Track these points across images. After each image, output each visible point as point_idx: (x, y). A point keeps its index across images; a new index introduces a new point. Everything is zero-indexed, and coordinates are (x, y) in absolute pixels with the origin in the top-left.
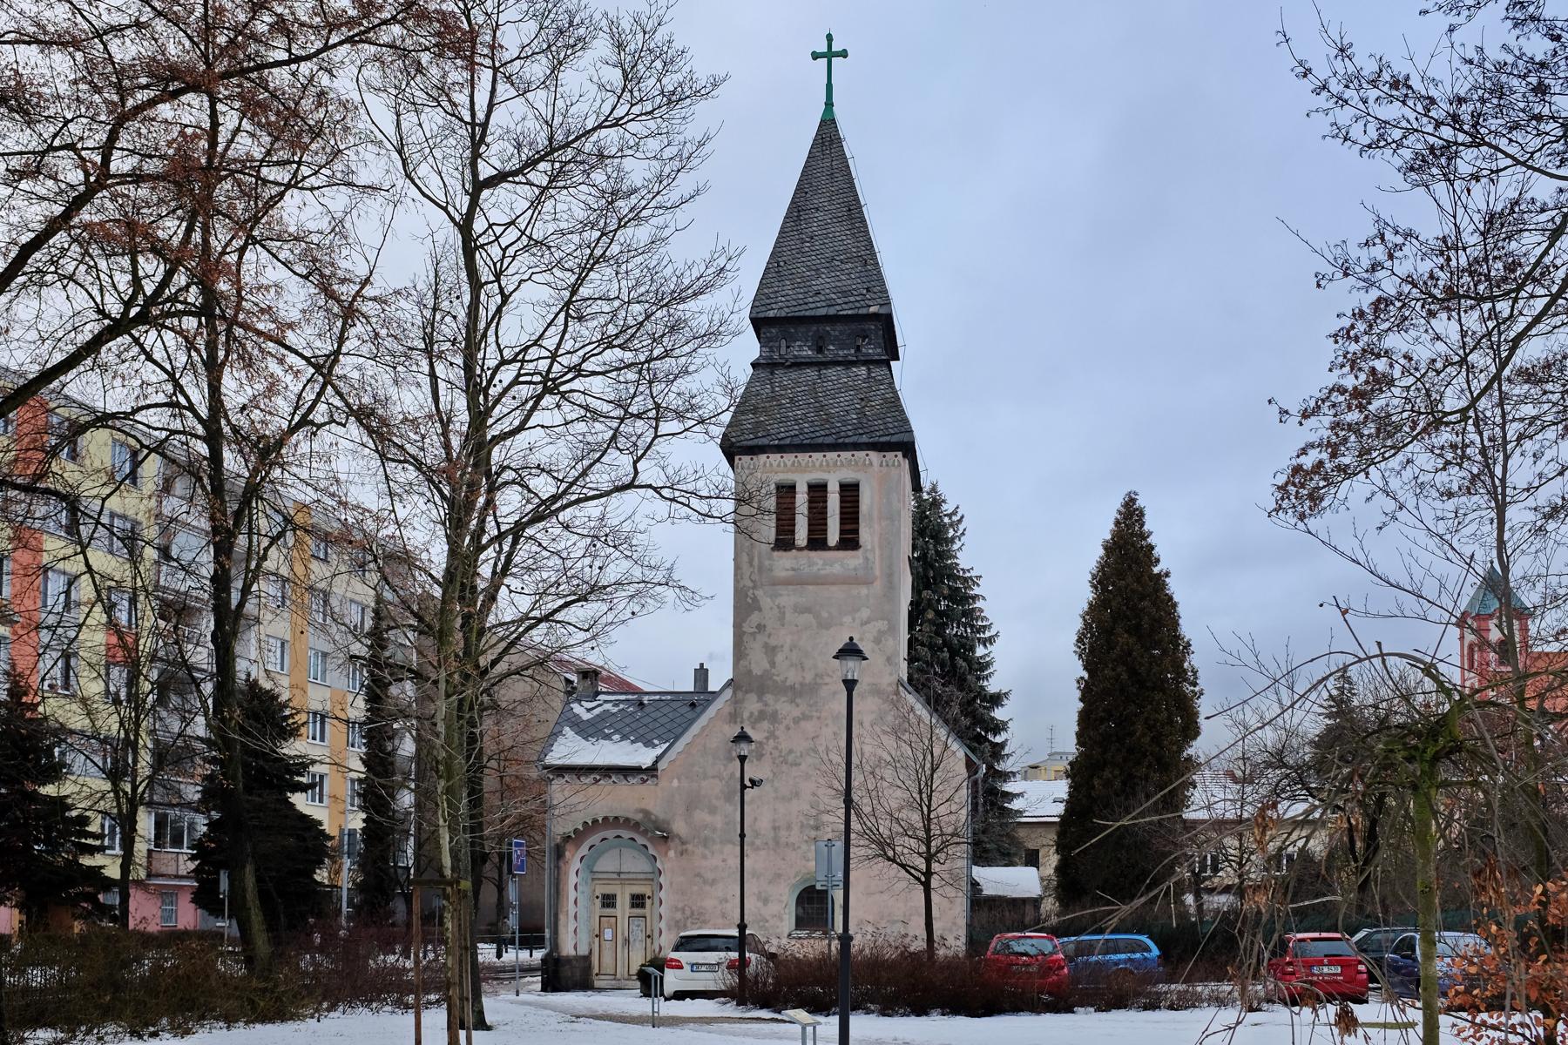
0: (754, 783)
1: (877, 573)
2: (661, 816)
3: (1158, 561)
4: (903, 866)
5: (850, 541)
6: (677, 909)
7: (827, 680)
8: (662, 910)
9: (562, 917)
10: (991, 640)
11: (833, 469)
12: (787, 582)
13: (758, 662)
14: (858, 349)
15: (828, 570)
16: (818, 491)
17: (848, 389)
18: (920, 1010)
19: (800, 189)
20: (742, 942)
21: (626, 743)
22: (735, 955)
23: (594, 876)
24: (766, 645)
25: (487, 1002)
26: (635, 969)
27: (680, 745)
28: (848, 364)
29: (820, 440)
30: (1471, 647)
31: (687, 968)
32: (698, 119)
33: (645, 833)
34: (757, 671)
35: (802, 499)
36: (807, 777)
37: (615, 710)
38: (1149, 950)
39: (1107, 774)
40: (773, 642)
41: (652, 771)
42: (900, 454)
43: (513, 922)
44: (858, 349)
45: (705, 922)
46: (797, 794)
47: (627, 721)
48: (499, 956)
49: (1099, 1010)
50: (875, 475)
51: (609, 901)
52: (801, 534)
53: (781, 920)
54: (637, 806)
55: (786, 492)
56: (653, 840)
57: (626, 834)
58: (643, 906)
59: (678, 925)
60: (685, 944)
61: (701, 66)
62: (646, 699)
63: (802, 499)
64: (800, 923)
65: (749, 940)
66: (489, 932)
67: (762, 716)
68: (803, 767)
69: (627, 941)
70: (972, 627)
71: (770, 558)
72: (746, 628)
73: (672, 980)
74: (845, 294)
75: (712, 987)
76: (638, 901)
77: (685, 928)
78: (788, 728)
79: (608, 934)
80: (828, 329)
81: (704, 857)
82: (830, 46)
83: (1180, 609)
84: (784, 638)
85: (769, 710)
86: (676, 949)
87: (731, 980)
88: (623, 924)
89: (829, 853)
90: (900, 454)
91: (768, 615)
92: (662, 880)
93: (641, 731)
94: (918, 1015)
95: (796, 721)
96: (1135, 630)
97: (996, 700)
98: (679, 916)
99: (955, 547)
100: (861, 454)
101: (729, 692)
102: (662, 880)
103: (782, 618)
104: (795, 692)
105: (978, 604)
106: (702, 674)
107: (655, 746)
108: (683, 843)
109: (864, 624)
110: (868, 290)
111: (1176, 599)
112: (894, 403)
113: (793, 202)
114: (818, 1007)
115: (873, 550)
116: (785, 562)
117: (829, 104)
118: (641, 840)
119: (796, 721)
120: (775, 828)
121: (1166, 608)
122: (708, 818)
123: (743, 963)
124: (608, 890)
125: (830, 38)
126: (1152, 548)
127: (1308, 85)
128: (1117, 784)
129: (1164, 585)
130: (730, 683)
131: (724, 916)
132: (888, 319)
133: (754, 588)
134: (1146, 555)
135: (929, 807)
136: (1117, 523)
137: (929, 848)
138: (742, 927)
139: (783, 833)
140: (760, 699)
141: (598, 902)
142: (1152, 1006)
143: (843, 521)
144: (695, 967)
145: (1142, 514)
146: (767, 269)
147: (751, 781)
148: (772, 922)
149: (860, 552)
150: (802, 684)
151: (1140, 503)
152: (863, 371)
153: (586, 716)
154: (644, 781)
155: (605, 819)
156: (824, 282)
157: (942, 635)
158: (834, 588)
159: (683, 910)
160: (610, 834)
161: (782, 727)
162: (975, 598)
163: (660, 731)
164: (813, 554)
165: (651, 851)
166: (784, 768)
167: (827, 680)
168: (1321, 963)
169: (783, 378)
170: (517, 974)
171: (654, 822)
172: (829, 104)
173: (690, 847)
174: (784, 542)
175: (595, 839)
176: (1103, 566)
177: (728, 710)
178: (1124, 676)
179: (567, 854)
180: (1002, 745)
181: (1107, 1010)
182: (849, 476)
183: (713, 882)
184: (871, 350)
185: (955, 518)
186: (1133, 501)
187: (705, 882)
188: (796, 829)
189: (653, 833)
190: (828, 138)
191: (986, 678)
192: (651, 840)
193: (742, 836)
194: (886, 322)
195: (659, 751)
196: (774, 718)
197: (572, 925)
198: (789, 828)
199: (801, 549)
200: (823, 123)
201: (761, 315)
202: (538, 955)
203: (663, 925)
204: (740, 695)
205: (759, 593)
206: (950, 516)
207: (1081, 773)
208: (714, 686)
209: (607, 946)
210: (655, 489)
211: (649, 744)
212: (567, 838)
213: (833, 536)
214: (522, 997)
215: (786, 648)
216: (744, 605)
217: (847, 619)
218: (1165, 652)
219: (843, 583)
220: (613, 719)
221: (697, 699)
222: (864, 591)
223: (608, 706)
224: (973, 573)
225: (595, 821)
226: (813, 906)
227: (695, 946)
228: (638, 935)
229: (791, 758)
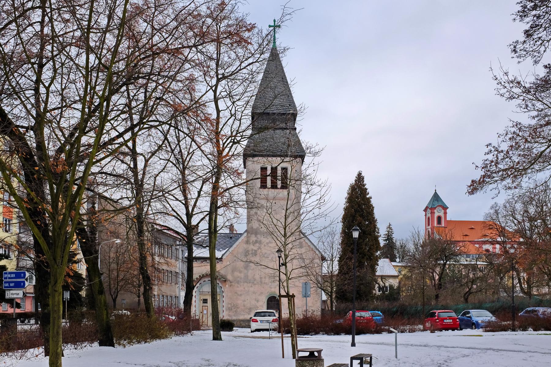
3: (368, 193)
8: (224, 304)
16: (274, 170)
18: (338, 333)
30: (429, 218)
31: (259, 322)
34: (255, 227)
55: (264, 169)
58: (207, 303)
67: (256, 242)
78: (265, 246)
79: (205, 312)
81: (238, 287)
85: (259, 240)
86: (255, 316)
92: (224, 294)
96: (362, 216)
98: (230, 306)
101: (246, 234)
102: (224, 294)
111: (374, 205)
114: (348, 333)
116: (265, 191)
119: (267, 243)
120: (261, 278)
122: (239, 275)
124: (205, 298)
127: (496, 82)
129: (370, 201)
130: (246, 231)
134: (364, 191)
139: (263, 279)
140: (256, 236)
141: (202, 302)
145: (363, 178)
151: (363, 175)
161: (263, 246)
164: (273, 190)
166: (264, 258)
168: (446, 319)
173: (233, 284)
177: (245, 239)
183: (241, 295)
187: (238, 295)
192: (221, 282)
196: (260, 242)
199: (269, 188)
203: (224, 309)
204: (249, 235)
209: (205, 316)
218: (370, 223)
229: (266, 256)
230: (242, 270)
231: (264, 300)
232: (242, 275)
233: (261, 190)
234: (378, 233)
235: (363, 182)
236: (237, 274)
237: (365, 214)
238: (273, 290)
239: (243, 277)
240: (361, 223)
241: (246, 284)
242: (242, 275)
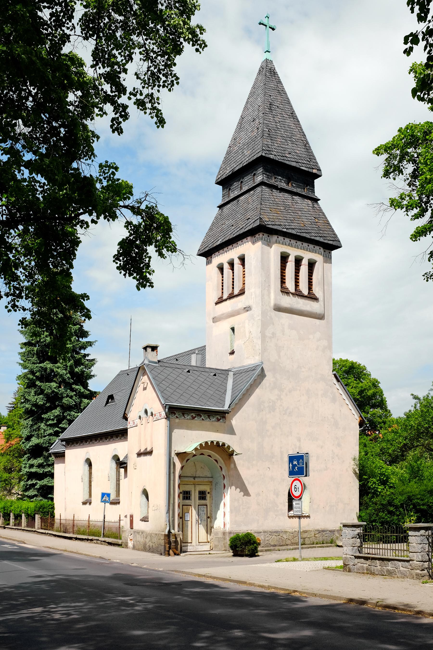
78: (287, 395)
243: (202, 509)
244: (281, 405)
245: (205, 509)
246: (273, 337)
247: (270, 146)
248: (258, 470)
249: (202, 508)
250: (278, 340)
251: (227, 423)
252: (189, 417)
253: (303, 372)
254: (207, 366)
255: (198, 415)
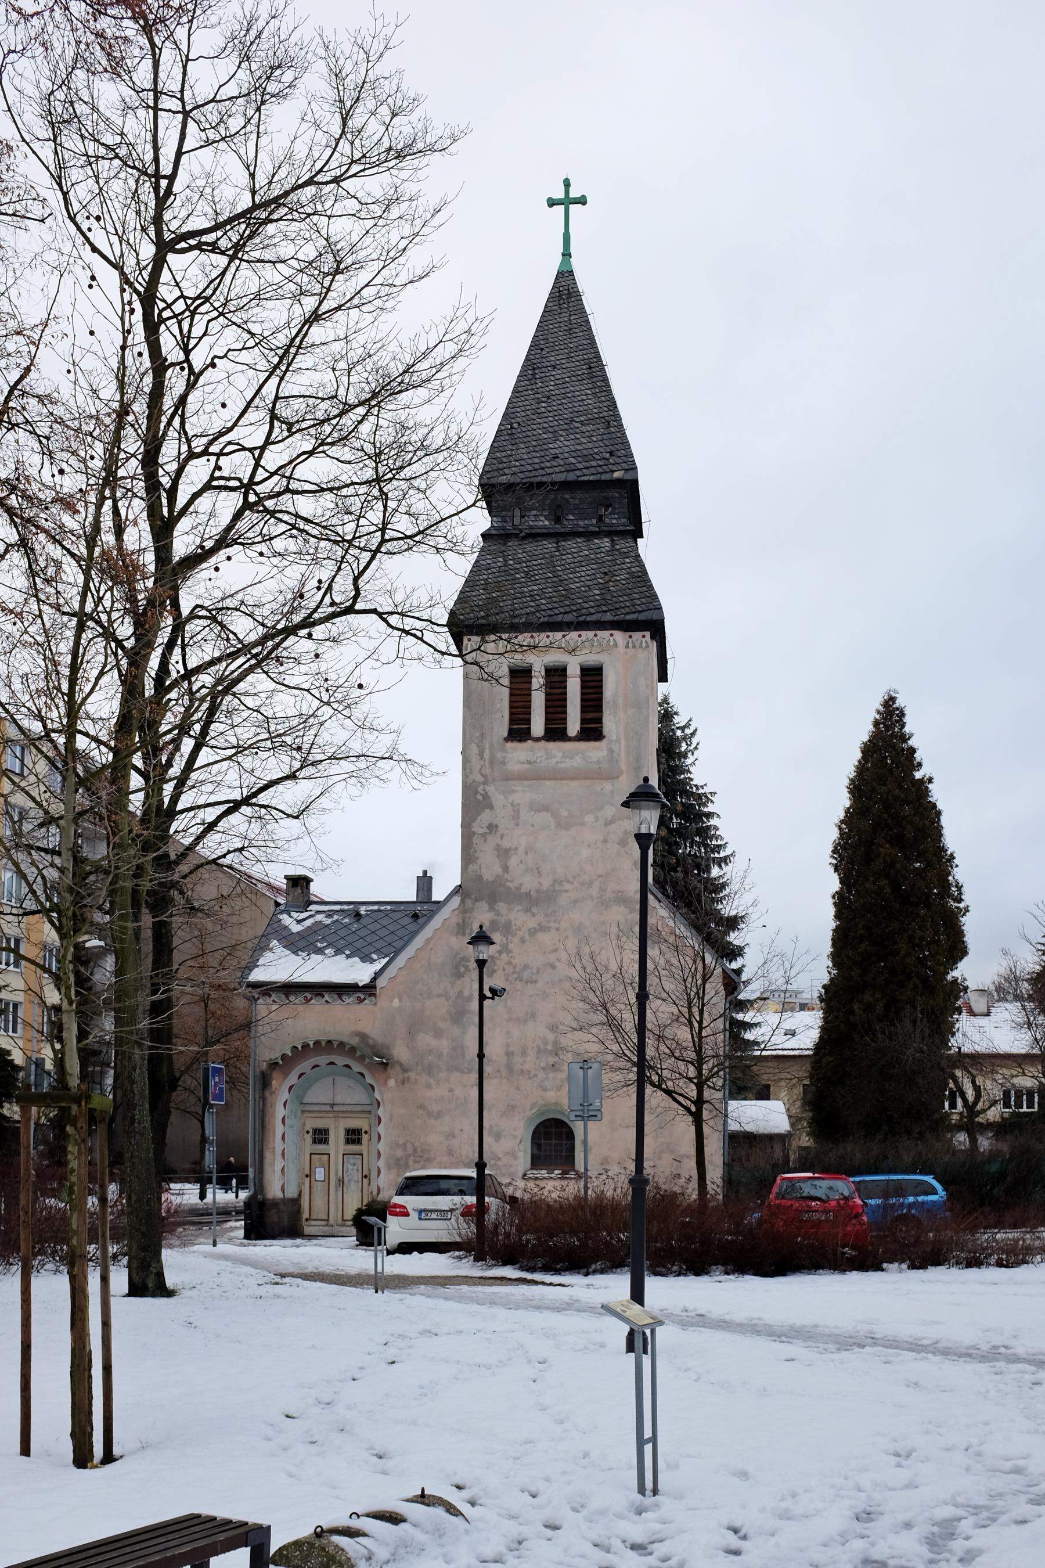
0: (494, 992)
1: (623, 766)
2: (380, 1040)
3: (920, 765)
4: (668, 1092)
5: (592, 731)
6: (398, 1145)
7: (567, 886)
8: (381, 1146)
9: (268, 1155)
10: (726, 860)
11: (572, 651)
12: (522, 777)
13: (489, 867)
14: (600, 519)
15: (568, 764)
17: (589, 561)
18: (698, 1268)
19: (535, 345)
20: (480, 1185)
21: (341, 958)
22: (471, 1200)
23: (304, 1108)
24: (498, 848)
25: (168, 1256)
26: (350, 1213)
27: (401, 960)
28: (589, 535)
29: (559, 618)
31: (414, 1215)
32: (427, 180)
33: (362, 1059)
34: (488, 876)
35: (538, 681)
36: (545, 995)
37: (328, 921)
38: (934, 1192)
39: (867, 997)
40: (506, 844)
41: (370, 988)
42: (648, 634)
43: (210, 1161)
44: (600, 519)
45: (428, 1160)
46: (533, 1015)
47: (342, 933)
48: (203, 1196)
49: (913, 1267)
50: (618, 655)
51: (320, 1136)
52: (538, 726)
53: (516, 1158)
54: (352, 1028)
56: (370, 1067)
57: (341, 1060)
58: (359, 1142)
59: (399, 1164)
60: (412, 1186)
61: (436, 115)
62: (363, 910)
63: (538, 681)
64: (537, 1161)
65: (488, 1182)
66: (195, 1172)
68: (539, 985)
69: (341, 1182)
70: (706, 846)
71: (504, 750)
72: (476, 828)
73: (396, 1230)
74: (586, 458)
75: (445, 1238)
76: (353, 1136)
77: (407, 1167)
78: (523, 941)
79: (320, 1174)
80: (565, 516)
81: (429, 1086)
82: (567, 192)
83: (944, 820)
84: (517, 838)
85: (502, 920)
86: (401, 1192)
87: (468, 1230)
88: (336, 1162)
89: (585, 1075)
90: (648, 634)
91: (500, 813)
93: (358, 945)
94: (697, 1274)
95: (532, 932)
96: (898, 841)
97: (733, 923)
98: (399, 1153)
99: (688, 761)
100: (604, 634)
101: (456, 900)
103: (516, 815)
104: (531, 900)
105: (713, 822)
106: (425, 882)
107: (372, 961)
108: (405, 1070)
109: (608, 823)
110: (611, 453)
111: (940, 806)
112: (641, 577)
113: (527, 359)
115: (618, 741)
116: (519, 754)
117: (567, 254)
118: (357, 1067)
119: (532, 932)
120: (509, 1054)
121: (928, 818)
122: (434, 1043)
123: (481, 1208)
124: (320, 1124)
125: (567, 184)
126: (913, 751)
128: (879, 1008)
130: (458, 890)
131: (450, 1153)
132: (635, 483)
133: (485, 783)
134: (908, 759)
135: (700, 1023)
136: (876, 723)
137: (699, 1070)
138: (481, 1166)
139: (517, 1059)
140: (492, 908)
141: (308, 1138)
142: (973, 1262)
143: (584, 709)
144: (423, 1213)
145: (902, 714)
146: (499, 431)
147: (491, 990)
148: (504, 1160)
149: (603, 744)
150: (538, 892)
152: (606, 543)
153: (296, 928)
154: (361, 1001)
155: (317, 1043)
156: (563, 446)
157: (674, 854)
158: (574, 784)
159: (404, 1146)
160: (322, 1060)
161: (516, 940)
162: (709, 815)
163: (378, 945)
164: (551, 745)
165: (369, 1079)
166: (519, 985)
167: (567, 886)
169: (518, 550)
170: (214, 1218)
171: (373, 1047)
172: (567, 254)
173: (412, 1075)
174: (519, 731)
175: (305, 1066)
176: (861, 769)
177: (455, 920)
178: (888, 890)
179: (274, 1082)
180: (738, 972)
181: (922, 1266)
182: (592, 659)
183: (439, 1115)
184: (616, 520)
185: (688, 731)
186: (893, 699)
187: (430, 1114)
188: (531, 1056)
189: (370, 1059)
190: (565, 295)
191: (720, 900)
193: (481, 1056)
194: (631, 489)
195: (378, 966)
197: (279, 1165)
198: (524, 1053)
199: (537, 740)
200: (560, 275)
201: (493, 481)
202: (243, 1195)
203: (381, 1163)
204: (469, 903)
205: (491, 789)
206: (683, 729)
207: (835, 999)
208: (439, 894)
209: (319, 1188)
210: (380, 615)
211: (366, 958)
212: (273, 1065)
213: (574, 726)
214: (221, 1248)
215: (521, 851)
216: (474, 802)
217: (589, 818)
218: (929, 864)
219: (586, 778)
220: (327, 932)
221: (420, 910)
222: (608, 786)
223: (319, 917)
224: (707, 790)
225: (305, 1046)
226: (553, 1142)
227: (423, 1189)
228: (353, 1174)
229: (526, 975)
230: (441, 1025)
231: (520, 1133)
232: (444, 1045)
233: (510, 745)
234: (960, 901)
235: (903, 726)
236: (425, 1040)
237: (910, 834)
238: (551, 1096)
239: (445, 1051)
240: (892, 865)
241: (456, 1076)
242: (444, 1045)
243: (352, 1161)
244: (510, 963)
245: (359, 1163)
246: (491, 833)
247: (504, 460)
248: (451, 1090)
249: (352, 1159)
250: (502, 837)
251: (379, 1004)
252: (351, 999)
253: (566, 891)
254: (433, 899)
255: (317, 995)
